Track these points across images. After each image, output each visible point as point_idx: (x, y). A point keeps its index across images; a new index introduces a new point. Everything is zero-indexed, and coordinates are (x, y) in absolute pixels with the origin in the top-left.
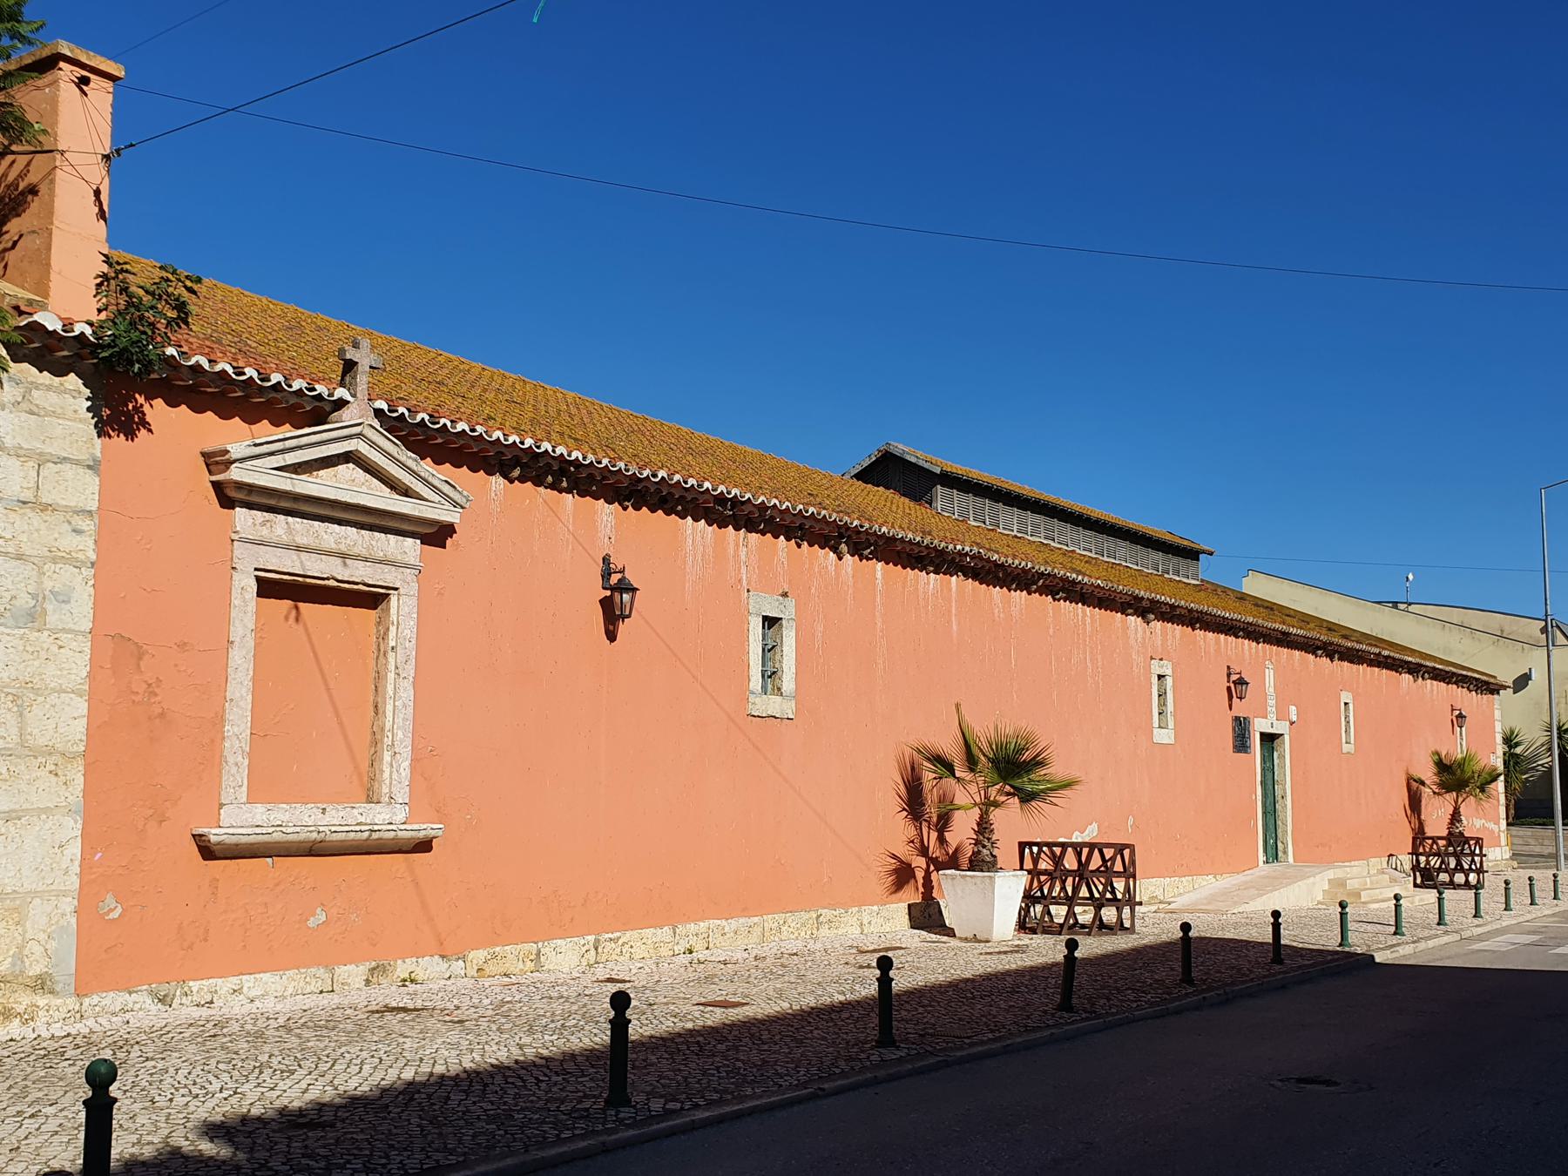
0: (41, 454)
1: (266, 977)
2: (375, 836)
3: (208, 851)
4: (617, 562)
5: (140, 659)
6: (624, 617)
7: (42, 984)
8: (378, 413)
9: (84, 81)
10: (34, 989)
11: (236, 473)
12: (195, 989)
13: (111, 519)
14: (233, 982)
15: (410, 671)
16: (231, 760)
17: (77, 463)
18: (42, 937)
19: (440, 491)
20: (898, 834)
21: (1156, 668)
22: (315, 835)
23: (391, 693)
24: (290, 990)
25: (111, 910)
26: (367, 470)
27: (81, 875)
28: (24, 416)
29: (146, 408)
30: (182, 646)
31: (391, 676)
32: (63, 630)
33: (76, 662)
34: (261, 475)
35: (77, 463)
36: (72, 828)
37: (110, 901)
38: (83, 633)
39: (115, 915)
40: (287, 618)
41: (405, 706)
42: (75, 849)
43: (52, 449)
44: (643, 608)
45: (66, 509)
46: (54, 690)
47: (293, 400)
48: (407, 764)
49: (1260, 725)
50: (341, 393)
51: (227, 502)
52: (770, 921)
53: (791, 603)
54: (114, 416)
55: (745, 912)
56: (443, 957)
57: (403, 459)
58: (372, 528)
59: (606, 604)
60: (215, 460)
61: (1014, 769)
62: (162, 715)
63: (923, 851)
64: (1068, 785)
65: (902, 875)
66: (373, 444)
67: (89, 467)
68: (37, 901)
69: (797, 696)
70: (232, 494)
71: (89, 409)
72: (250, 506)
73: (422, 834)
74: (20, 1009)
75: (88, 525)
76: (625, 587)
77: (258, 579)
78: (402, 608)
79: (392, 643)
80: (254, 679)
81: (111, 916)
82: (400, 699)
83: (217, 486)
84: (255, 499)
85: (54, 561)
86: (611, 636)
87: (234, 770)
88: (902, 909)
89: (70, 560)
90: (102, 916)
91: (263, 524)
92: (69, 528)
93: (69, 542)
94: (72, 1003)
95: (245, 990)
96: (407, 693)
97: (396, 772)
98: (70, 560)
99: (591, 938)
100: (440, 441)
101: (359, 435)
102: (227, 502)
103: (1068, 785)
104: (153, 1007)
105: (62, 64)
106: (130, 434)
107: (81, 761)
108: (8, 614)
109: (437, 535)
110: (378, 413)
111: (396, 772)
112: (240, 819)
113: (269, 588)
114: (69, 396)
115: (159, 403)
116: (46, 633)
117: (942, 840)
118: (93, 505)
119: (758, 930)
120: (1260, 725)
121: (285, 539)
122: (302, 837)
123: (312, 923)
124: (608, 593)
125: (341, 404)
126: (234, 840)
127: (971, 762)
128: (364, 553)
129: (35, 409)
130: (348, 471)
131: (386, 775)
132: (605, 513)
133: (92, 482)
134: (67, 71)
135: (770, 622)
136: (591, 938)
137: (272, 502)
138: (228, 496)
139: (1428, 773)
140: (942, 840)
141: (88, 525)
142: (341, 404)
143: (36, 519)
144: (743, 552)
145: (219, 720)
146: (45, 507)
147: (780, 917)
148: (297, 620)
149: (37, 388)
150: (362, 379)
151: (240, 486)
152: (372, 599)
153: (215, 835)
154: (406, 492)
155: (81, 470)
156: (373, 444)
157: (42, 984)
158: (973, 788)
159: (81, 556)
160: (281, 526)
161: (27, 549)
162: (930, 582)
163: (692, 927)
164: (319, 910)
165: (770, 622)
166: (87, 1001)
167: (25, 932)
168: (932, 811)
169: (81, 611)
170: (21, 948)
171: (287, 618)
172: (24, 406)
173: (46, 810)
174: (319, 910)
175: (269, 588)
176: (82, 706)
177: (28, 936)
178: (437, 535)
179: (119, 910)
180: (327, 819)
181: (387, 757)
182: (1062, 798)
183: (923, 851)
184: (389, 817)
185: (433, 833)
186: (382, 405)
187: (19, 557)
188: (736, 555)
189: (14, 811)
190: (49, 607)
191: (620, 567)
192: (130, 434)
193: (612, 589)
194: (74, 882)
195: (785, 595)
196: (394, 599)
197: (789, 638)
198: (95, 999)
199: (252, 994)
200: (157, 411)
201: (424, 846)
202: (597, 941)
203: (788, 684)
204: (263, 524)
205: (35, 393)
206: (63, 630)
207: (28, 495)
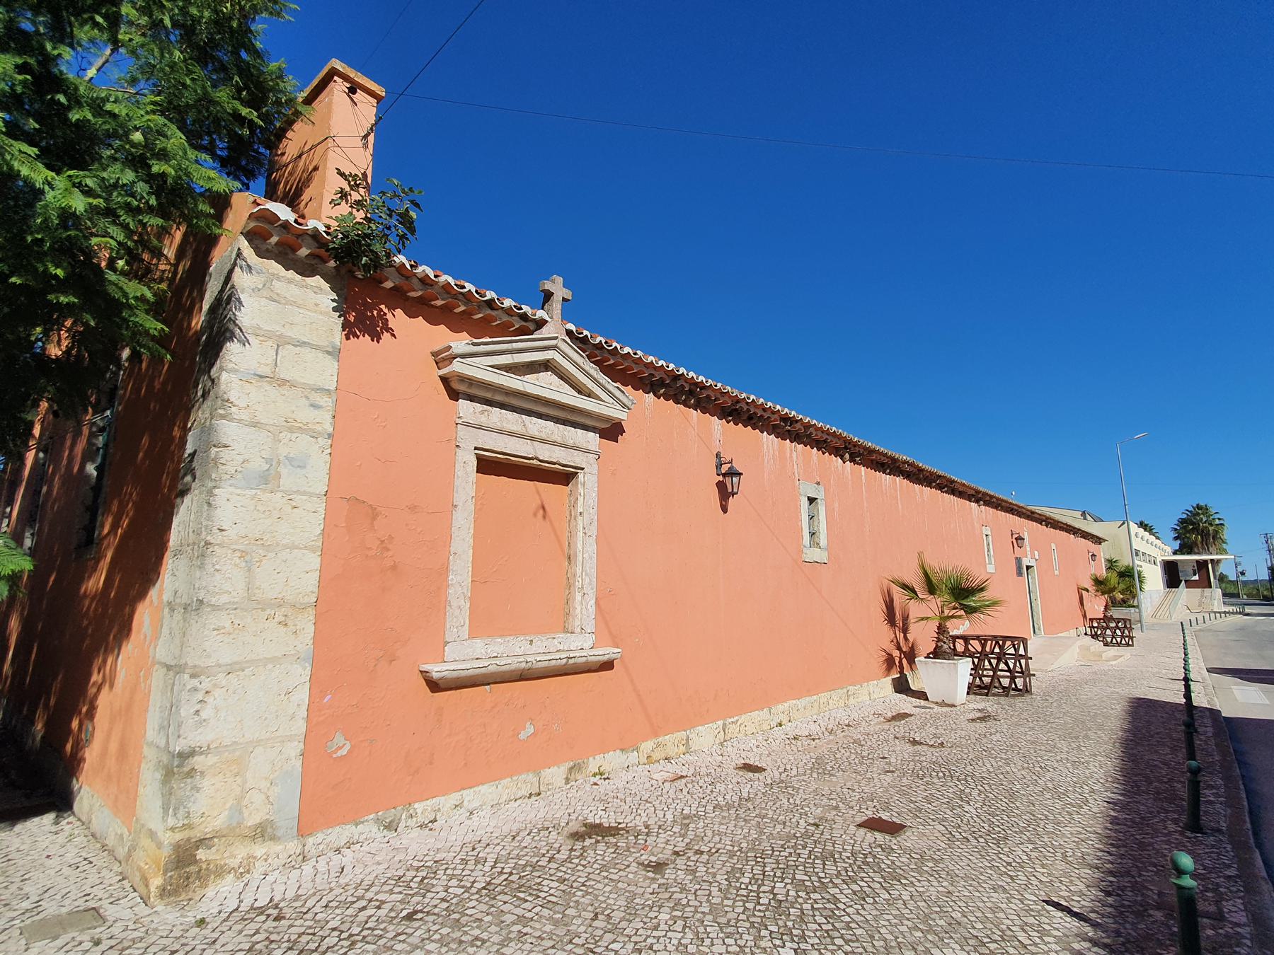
0: (280, 336)
1: (483, 789)
2: (571, 661)
3: (435, 686)
4: (726, 456)
5: (374, 518)
6: (733, 494)
7: (263, 832)
8: (569, 333)
9: (352, 90)
10: (253, 838)
11: (457, 367)
12: (419, 811)
13: (346, 399)
14: (454, 798)
15: (593, 531)
16: (454, 604)
17: (317, 348)
18: (264, 784)
19: (610, 400)
20: (884, 636)
21: (985, 532)
22: (523, 665)
23: (580, 547)
24: (504, 798)
25: (340, 748)
26: (561, 378)
27: (308, 719)
28: (264, 302)
29: (389, 316)
30: (413, 508)
31: (580, 534)
32: (297, 492)
33: (310, 521)
34: (479, 369)
35: (317, 348)
36: (301, 674)
37: (339, 739)
38: (318, 496)
39: (344, 752)
40: (535, 515)
41: (590, 558)
42: (303, 695)
43: (294, 333)
44: (744, 485)
45: (304, 386)
46: (286, 547)
47: (505, 318)
48: (593, 602)
49: (1026, 562)
50: (540, 314)
51: (454, 395)
52: (823, 697)
53: (821, 488)
54: (361, 319)
55: (810, 693)
56: (622, 750)
57: (587, 368)
58: (564, 422)
59: (721, 486)
60: (442, 358)
61: (964, 594)
62: (394, 568)
63: (899, 648)
64: (995, 603)
65: (890, 662)
66: (565, 356)
67: (328, 353)
68: (259, 750)
69: (828, 549)
70: (456, 386)
71: (335, 309)
72: (471, 398)
73: (605, 658)
74: (234, 863)
75: (327, 402)
76: (733, 473)
77: (479, 458)
78: (588, 484)
79: (580, 510)
80: (474, 536)
81: (339, 753)
82: (586, 548)
83: (445, 380)
84: (474, 391)
85: (291, 430)
86: (725, 510)
87: (457, 612)
88: (889, 679)
89: (304, 429)
90: (330, 755)
91: (482, 412)
92: (307, 403)
93: (306, 415)
94: (293, 846)
95: (465, 803)
96: (592, 548)
97: (584, 609)
98: (304, 429)
99: (720, 723)
100: (612, 362)
101: (554, 348)
102: (454, 395)
103: (995, 603)
104: (379, 835)
105: (336, 78)
106: (376, 337)
107: (312, 612)
108: (239, 476)
109: (612, 431)
110: (569, 333)
111: (584, 609)
112: (463, 653)
113: (489, 465)
114: (317, 296)
115: (399, 312)
116: (279, 495)
117: (906, 638)
118: (333, 386)
119: (816, 704)
120: (1026, 562)
121: (499, 426)
122: (513, 667)
123: (522, 736)
124: (721, 478)
125: (541, 324)
126: (455, 674)
127: (932, 589)
128: (559, 440)
129: (275, 297)
130: (547, 377)
131: (578, 611)
132: (716, 425)
133: (332, 366)
134: (339, 86)
135: (811, 500)
136: (720, 723)
137: (489, 395)
138: (455, 389)
139: (1088, 584)
140: (906, 638)
141: (327, 402)
142: (541, 324)
143: (273, 392)
144: (794, 455)
145: (444, 571)
146: (283, 383)
147: (827, 694)
148: (544, 517)
149: (278, 279)
150: (556, 304)
151: (463, 379)
152: (564, 477)
153: (438, 670)
154: (590, 395)
155: (320, 355)
156: (565, 356)
157: (263, 832)
158: (934, 606)
159: (318, 428)
160: (497, 416)
161: (262, 418)
162: (886, 479)
163: (780, 707)
164: (528, 725)
165: (811, 500)
166: (310, 840)
167: (245, 782)
168: (899, 622)
169: (317, 475)
170: (239, 799)
171: (535, 515)
172: (265, 293)
173: (274, 660)
174: (528, 725)
175: (489, 465)
176: (314, 561)
177: (248, 786)
178: (612, 431)
179: (348, 747)
180: (534, 649)
181: (578, 597)
182: (996, 612)
183: (899, 648)
184: (581, 644)
185: (614, 656)
186: (571, 327)
187: (254, 424)
188: (791, 457)
189: (235, 663)
190: (284, 470)
191: (729, 459)
192: (376, 337)
193: (724, 475)
194: (300, 726)
195: (818, 483)
196: (581, 476)
197: (822, 509)
198: (320, 836)
199: (471, 807)
200: (397, 319)
201: (607, 665)
202: (724, 725)
203: (823, 541)
204: (482, 412)
205: (276, 284)
206: (297, 492)
207: (266, 371)
